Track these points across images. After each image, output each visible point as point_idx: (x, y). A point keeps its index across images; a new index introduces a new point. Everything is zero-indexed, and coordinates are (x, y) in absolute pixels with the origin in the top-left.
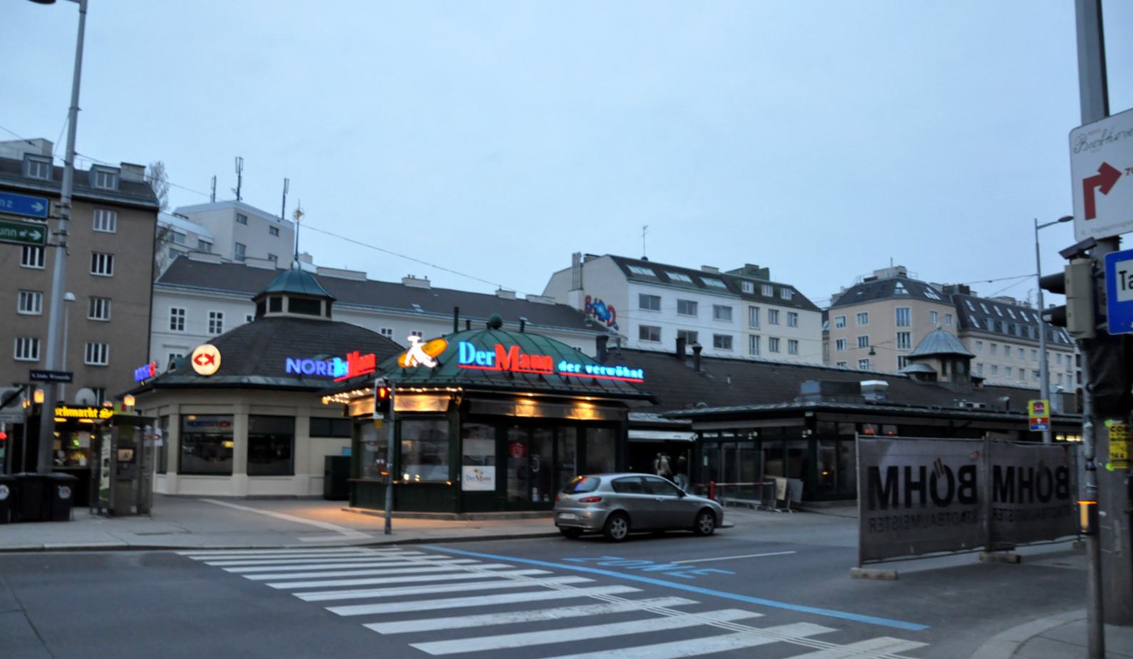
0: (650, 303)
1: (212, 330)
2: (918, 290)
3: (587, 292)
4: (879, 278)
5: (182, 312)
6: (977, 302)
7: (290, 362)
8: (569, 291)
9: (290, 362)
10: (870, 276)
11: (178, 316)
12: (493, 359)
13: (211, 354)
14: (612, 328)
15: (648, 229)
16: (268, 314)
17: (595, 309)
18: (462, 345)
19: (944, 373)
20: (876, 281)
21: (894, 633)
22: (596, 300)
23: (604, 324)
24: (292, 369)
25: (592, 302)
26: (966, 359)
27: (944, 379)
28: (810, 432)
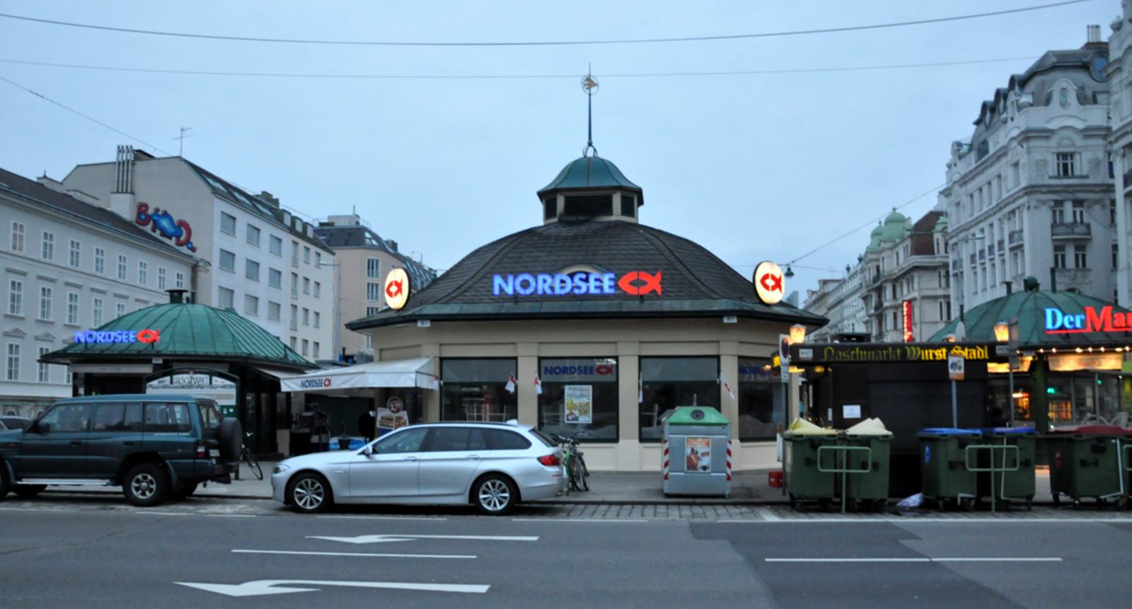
3: (142, 198)
4: (336, 225)
7: (498, 280)
8: (113, 193)
9: (498, 280)
10: (325, 220)
12: (1083, 322)
13: (778, 277)
15: (187, 133)
18: (1049, 312)
20: (332, 228)
24: (501, 289)
25: (150, 212)
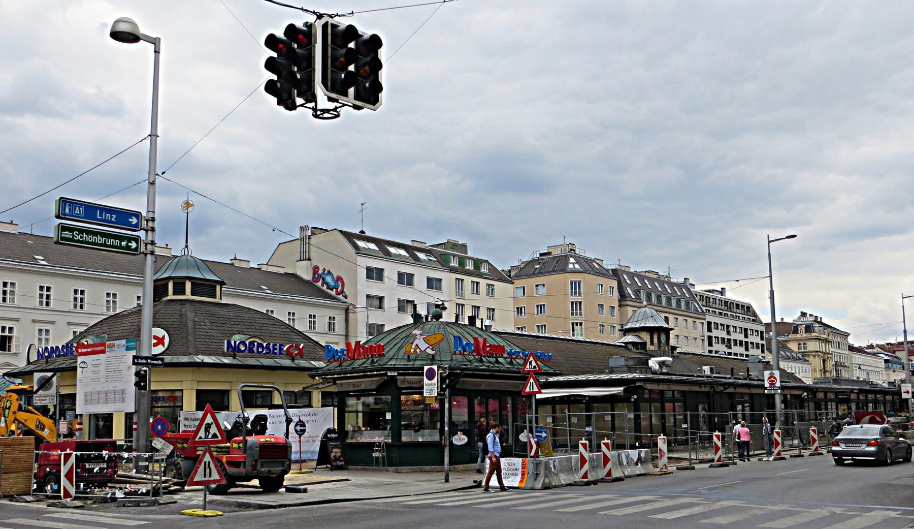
0: (375, 274)
1: (108, 309)
2: (590, 267)
5: (115, 295)
6: (632, 275)
11: (111, 299)
14: (340, 297)
16: (171, 296)
17: (323, 279)
19: (652, 343)
21: (878, 509)
22: (324, 270)
23: (333, 293)
26: (667, 331)
27: (652, 348)
28: (635, 397)
